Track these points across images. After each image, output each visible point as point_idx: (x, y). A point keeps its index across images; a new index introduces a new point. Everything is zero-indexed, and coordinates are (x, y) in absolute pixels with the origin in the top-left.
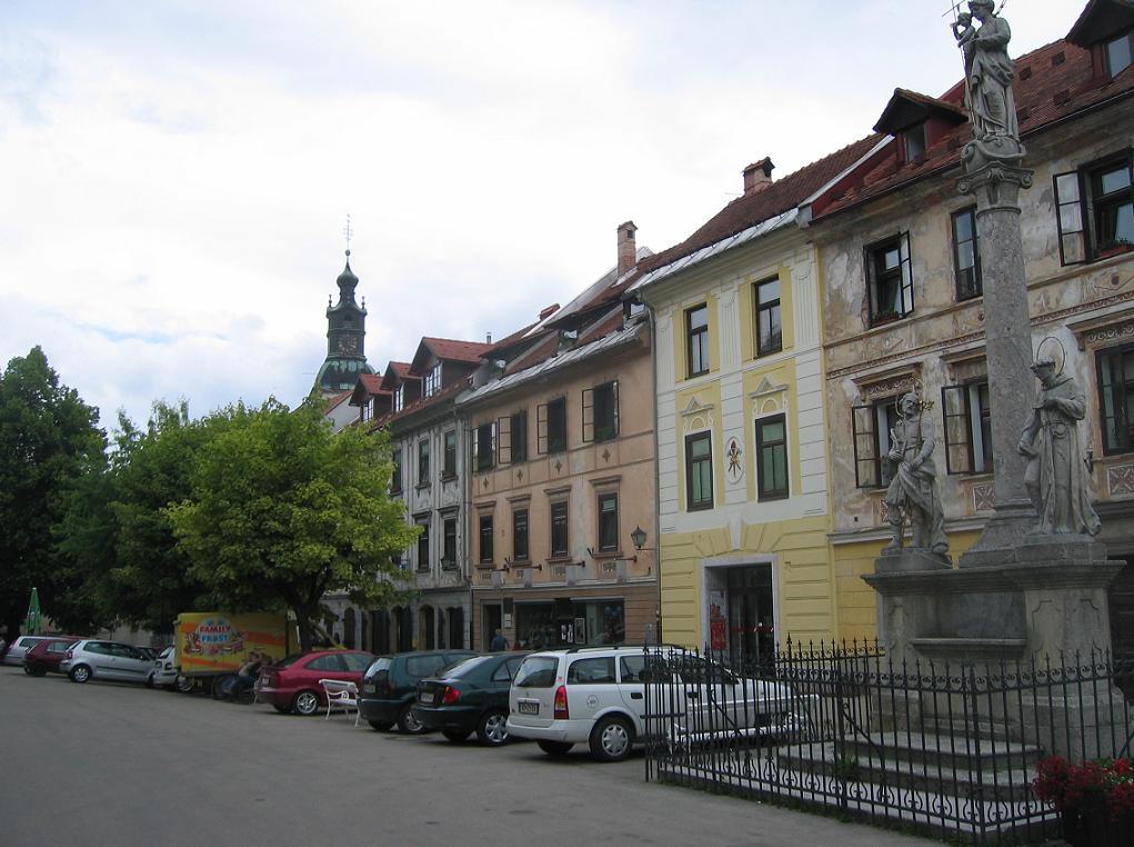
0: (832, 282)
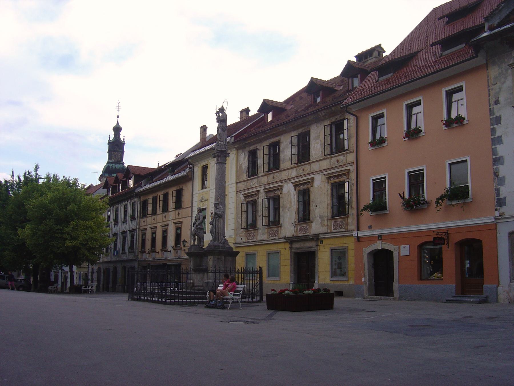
0: (240, 162)
